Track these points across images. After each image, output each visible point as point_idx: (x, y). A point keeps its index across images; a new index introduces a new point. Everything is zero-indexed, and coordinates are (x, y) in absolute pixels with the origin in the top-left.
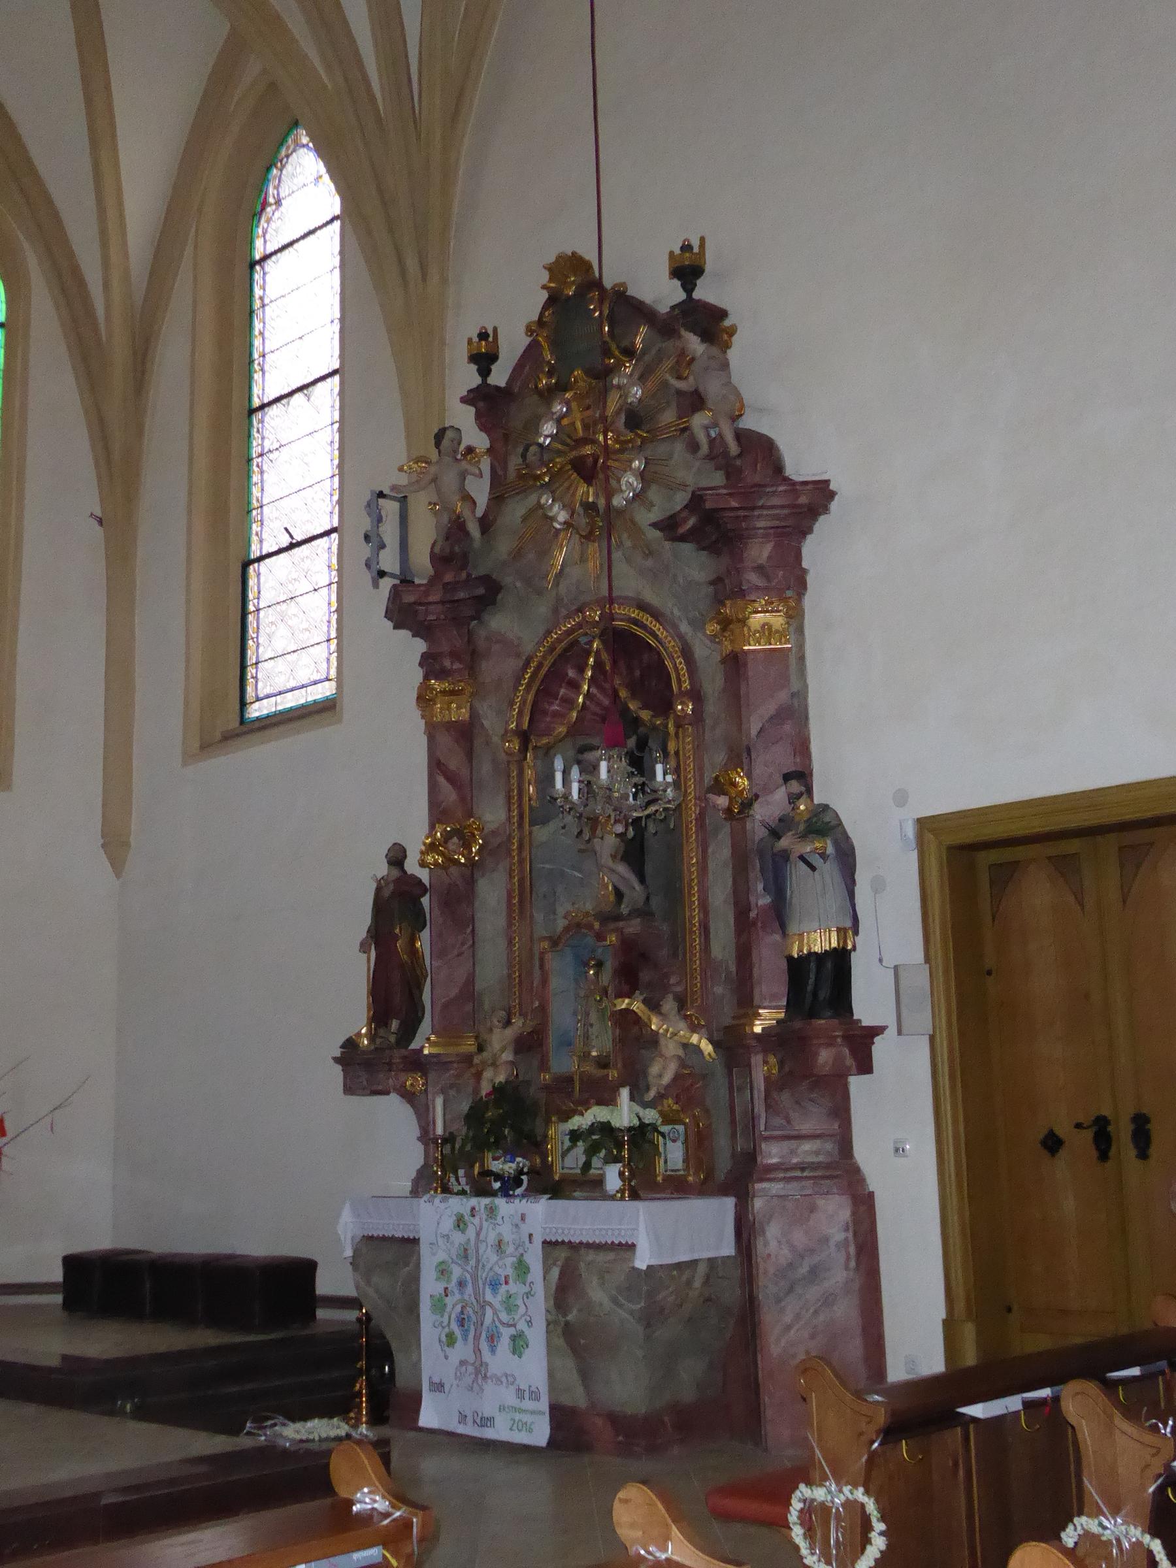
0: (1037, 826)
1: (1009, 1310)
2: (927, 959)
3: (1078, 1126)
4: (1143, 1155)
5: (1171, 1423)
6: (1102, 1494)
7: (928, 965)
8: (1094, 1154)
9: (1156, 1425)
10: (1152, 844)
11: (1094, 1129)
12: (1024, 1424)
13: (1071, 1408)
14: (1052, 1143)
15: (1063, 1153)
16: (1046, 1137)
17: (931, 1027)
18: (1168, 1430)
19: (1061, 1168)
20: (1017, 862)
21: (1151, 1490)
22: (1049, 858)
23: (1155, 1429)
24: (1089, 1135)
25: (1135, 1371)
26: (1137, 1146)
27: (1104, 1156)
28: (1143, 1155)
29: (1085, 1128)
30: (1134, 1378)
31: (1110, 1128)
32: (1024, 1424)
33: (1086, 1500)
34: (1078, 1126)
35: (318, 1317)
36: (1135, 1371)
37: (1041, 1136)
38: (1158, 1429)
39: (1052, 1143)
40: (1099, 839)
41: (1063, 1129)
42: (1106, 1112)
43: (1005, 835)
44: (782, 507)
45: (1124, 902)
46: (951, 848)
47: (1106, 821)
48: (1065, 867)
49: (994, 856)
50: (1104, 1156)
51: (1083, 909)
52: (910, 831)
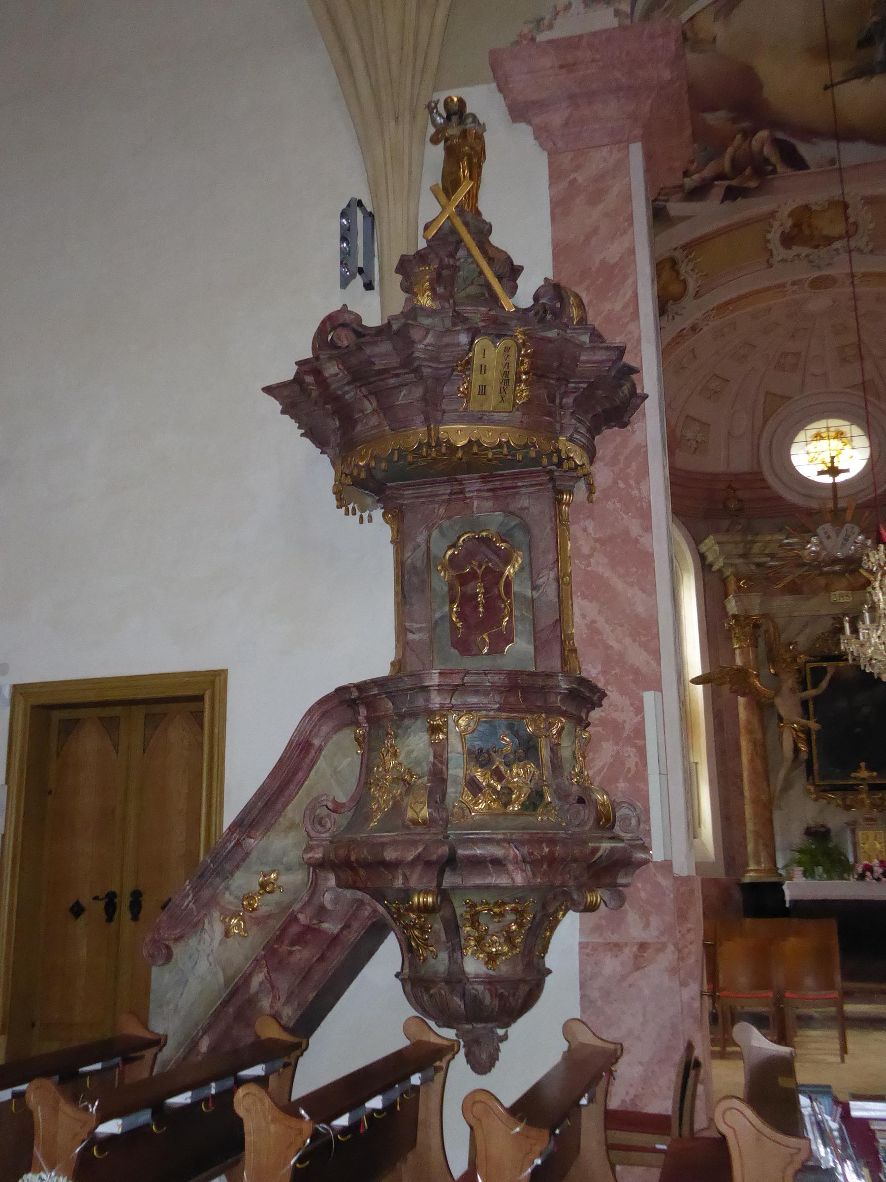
0: (92, 697)
1: (33, 1025)
2: (7, 782)
3: (96, 898)
4: (135, 917)
5: (97, 1103)
6: (44, 1156)
7: (7, 786)
8: (104, 916)
9: (87, 1106)
10: (165, 714)
11: (106, 900)
12: (13, 1109)
13: (32, 1099)
14: (77, 910)
15: (84, 917)
16: (73, 906)
17: (3, 830)
18: (94, 1108)
19: (81, 927)
20: (79, 719)
21: (78, 1150)
22: (100, 718)
23: (86, 1109)
24: (101, 905)
25: (98, 1066)
26: (132, 913)
27: (110, 918)
28: (135, 917)
29: (100, 900)
30: (97, 1071)
31: (116, 900)
32: (13, 1109)
33: (34, 1161)
34: (96, 898)
35: (746, 919)
36: (98, 1066)
37: (71, 905)
38: (88, 1109)
39: (77, 910)
40: (133, 708)
41: (86, 901)
42: (114, 888)
43: (118, 698)
44: (582, 442)
45: (144, 750)
46: (33, 707)
47: (139, 697)
48: (110, 726)
49: (66, 714)
50: (110, 918)
51: (117, 753)
52: (7, 693)
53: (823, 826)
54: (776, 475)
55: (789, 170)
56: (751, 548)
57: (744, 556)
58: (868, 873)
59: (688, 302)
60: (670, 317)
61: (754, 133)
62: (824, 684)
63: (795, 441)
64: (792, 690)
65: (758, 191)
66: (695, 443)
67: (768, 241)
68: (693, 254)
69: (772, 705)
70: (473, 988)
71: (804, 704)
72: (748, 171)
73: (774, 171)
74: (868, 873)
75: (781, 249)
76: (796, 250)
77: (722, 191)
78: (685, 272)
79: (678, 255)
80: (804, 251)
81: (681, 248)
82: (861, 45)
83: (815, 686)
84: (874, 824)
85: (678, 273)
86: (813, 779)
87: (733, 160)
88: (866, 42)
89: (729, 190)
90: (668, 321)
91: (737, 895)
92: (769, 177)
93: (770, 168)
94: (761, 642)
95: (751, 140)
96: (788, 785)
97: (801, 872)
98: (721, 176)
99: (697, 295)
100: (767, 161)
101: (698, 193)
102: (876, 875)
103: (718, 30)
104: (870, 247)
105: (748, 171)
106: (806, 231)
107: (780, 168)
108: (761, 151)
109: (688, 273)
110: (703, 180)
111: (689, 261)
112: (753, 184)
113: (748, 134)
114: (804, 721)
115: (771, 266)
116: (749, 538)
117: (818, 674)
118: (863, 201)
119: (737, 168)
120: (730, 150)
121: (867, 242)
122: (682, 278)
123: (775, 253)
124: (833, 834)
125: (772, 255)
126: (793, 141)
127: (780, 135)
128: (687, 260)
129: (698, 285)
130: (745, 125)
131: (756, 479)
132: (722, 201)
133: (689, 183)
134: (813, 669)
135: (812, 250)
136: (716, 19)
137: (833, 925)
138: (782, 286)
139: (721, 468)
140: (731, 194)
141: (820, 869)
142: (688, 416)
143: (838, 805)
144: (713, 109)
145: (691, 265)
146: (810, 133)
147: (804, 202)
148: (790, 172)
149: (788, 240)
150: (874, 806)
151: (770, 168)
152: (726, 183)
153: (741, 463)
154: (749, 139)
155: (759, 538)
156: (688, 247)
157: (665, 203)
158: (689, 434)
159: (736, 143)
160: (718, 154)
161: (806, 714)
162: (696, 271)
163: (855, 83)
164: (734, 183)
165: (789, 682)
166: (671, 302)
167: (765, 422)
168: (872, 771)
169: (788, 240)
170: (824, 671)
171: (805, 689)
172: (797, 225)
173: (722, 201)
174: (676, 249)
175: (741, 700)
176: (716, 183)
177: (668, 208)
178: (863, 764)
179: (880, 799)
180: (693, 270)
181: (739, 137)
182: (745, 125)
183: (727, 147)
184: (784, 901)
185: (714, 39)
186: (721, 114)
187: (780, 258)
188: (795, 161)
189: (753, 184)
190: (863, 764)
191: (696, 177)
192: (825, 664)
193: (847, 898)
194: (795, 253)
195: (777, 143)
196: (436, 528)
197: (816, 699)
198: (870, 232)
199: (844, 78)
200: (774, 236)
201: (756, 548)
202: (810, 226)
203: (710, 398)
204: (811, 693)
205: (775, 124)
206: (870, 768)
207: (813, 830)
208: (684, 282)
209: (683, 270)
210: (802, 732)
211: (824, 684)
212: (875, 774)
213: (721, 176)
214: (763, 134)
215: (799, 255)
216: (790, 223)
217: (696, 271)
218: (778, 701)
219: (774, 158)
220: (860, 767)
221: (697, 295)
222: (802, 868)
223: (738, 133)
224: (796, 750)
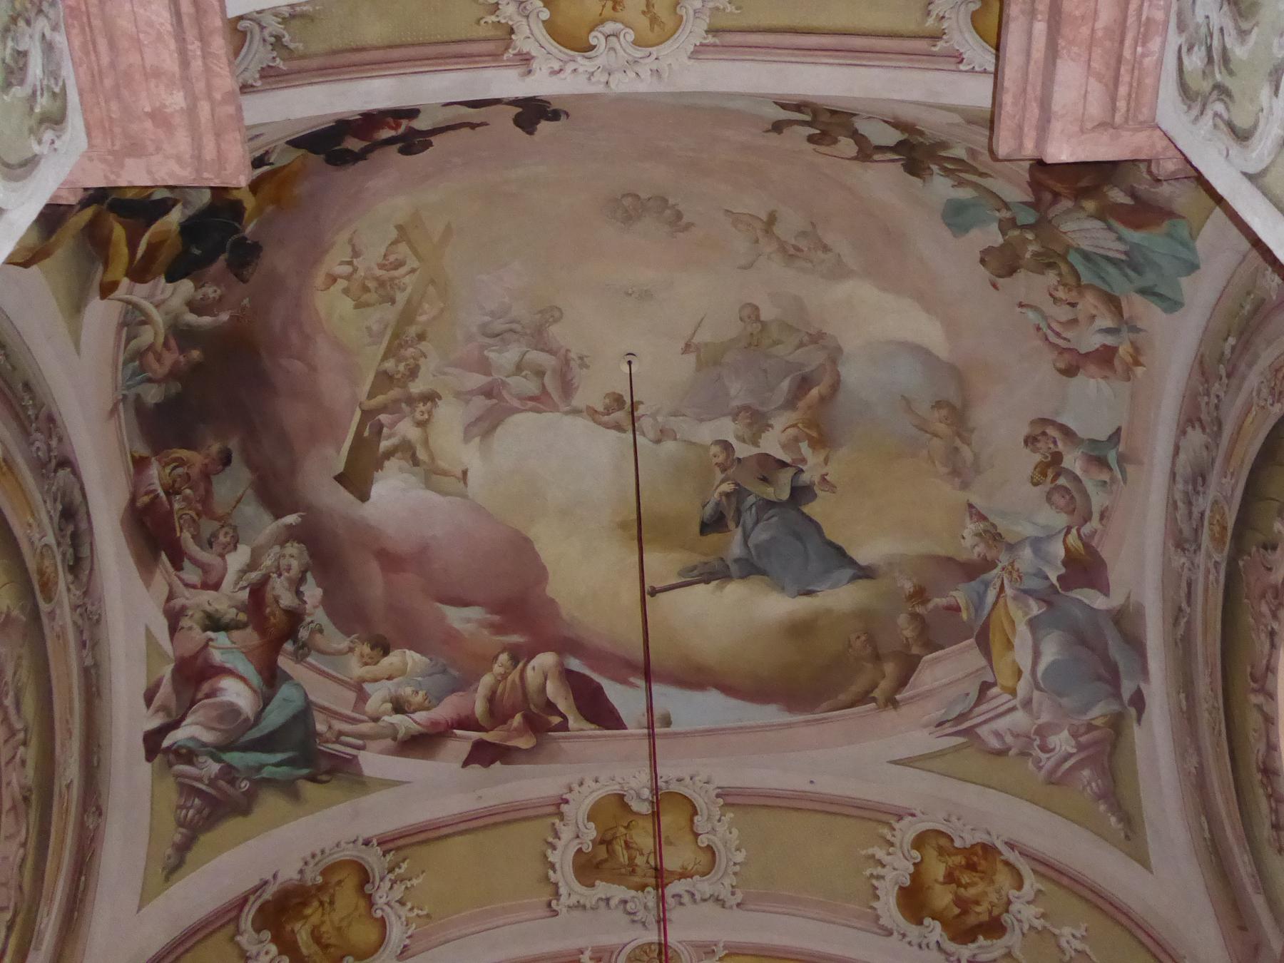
61: (531, 656)
65: (530, 755)
67: (552, 866)
68: (404, 866)
72: (518, 719)
73: (564, 726)
75: (577, 886)
76: (603, 888)
78: (388, 904)
79: (374, 860)
80: (618, 892)
81: (379, 844)
82: (705, 528)
84: (251, 32)
85: (371, 903)
87: (491, 699)
88: (714, 524)
98: (467, 723)
100: (551, 707)
103: (470, 456)
104: (739, 896)
106: (623, 856)
108: (543, 689)
109: (391, 907)
110: (435, 724)
112: (524, 742)
113: (519, 656)
118: (721, 801)
119: (497, 713)
120: (487, 680)
122: (379, 914)
123: (563, 890)
125: (557, 895)
126: (596, 677)
127: (575, 664)
128: (391, 876)
129: (409, 933)
130: (515, 639)
132: (466, 764)
136: (467, 438)
140: (483, 754)
145: (399, 891)
147: (615, 788)
148: (591, 730)
149: (588, 868)
151: (556, 720)
152: (475, 735)
154: (521, 665)
156: (392, 843)
157: (354, 752)
159: (497, 669)
160: (465, 684)
162: (409, 905)
163: (701, 591)
169: (588, 868)
172: (605, 841)
173: (466, 764)
174: (367, 843)
176: (458, 732)
177: (360, 758)
180: (402, 902)
181: (504, 657)
182: (515, 639)
185: (465, 473)
186: (475, 613)
189: (524, 742)
191: (421, 716)
195: (569, 677)
196: (181, 530)
198: (737, 868)
200: (563, 857)
202: (627, 846)
205: (567, 645)
208: (382, 922)
209: (380, 899)
213: (467, 723)
214: (546, 660)
215: (608, 900)
216: (591, 832)
217: (409, 905)
219: (564, 703)
223: (502, 652)
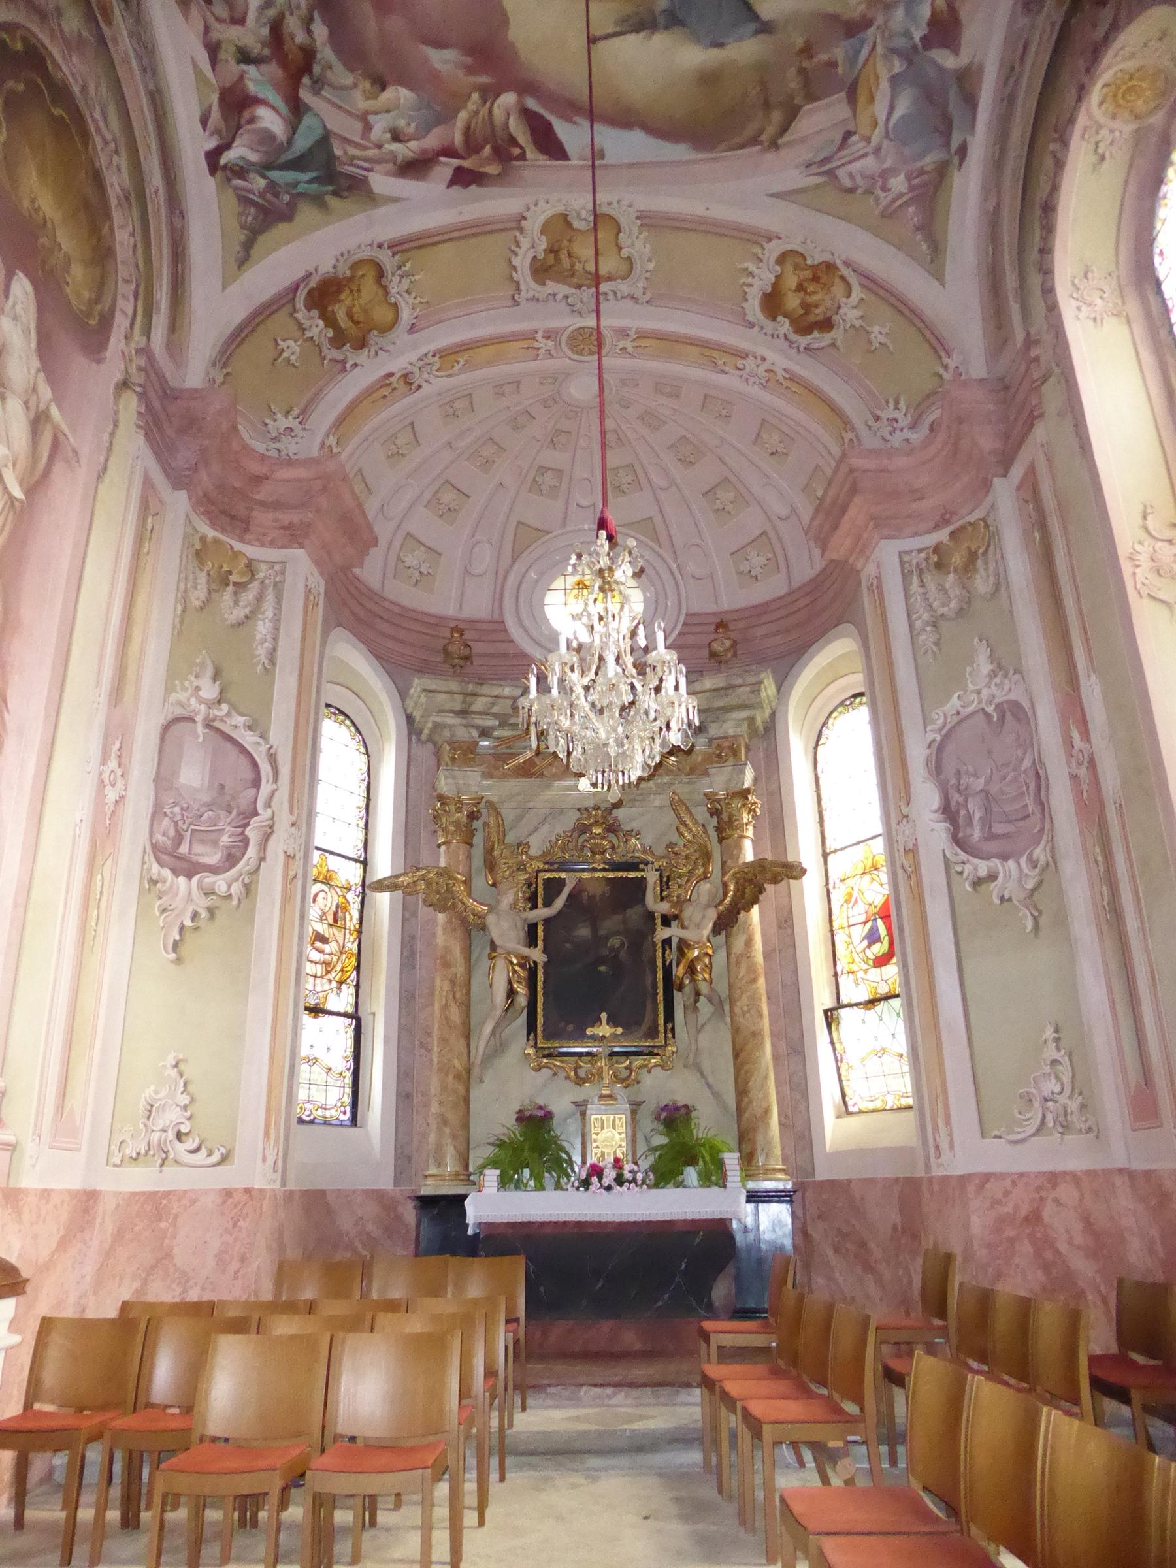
53: (540, 1108)
54: (520, 621)
55: (541, 157)
56: (471, 704)
57: (463, 713)
58: (595, 1179)
59: (400, 335)
60: (373, 352)
62: (560, 902)
63: (552, 587)
64: (514, 906)
66: (417, 574)
67: (515, 268)
68: (408, 265)
69: (483, 928)
70: (311, 1308)
71: (532, 929)
72: (487, 150)
73: (522, 157)
74: (595, 1179)
75: (533, 285)
76: (551, 287)
77: (448, 173)
79: (386, 259)
80: (562, 289)
83: (548, 903)
86: (536, 1039)
87: (467, 132)
89: (459, 170)
90: (369, 356)
91: (410, 1214)
92: (514, 163)
93: (517, 151)
94: (478, 840)
95: (492, 104)
96: (498, 1048)
97: (495, 1178)
98: (449, 152)
99: (412, 329)
100: (513, 141)
101: (414, 168)
102: (606, 1181)
105: (487, 150)
107: (531, 153)
108: (506, 125)
110: (424, 151)
111: (402, 277)
113: (489, 94)
114: (526, 951)
115: (516, 303)
116: (471, 687)
117: (553, 887)
119: (472, 146)
120: (463, 115)
121: (644, 289)
122: (393, 300)
123: (523, 287)
124: (555, 1121)
125: (518, 290)
126: (548, 115)
127: (531, 104)
128: (399, 272)
130: (484, 79)
131: (496, 628)
132: (448, 186)
133: (404, 151)
134: (547, 882)
135: (573, 290)
137: (517, 1269)
138: (530, 336)
139: (449, 609)
140: (462, 178)
141: (526, 1172)
142: (409, 535)
143: (567, 1078)
144: (439, 44)
145: (406, 283)
146: (571, 109)
148: (542, 160)
149: (542, 271)
150: (617, 1078)
151: (516, 151)
152: (456, 162)
153: (477, 606)
154: (488, 104)
155: (484, 690)
156: (399, 246)
157: (365, 173)
158: (410, 560)
159: (471, 106)
160: (444, 117)
161: (532, 941)
164: (466, 164)
165: (511, 895)
166: (375, 332)
167: (514, 560)
168: (616, 1025)
169: (542, 271)
170: (561, 883)
171: (534, 907)
172: (553, 251)
173: (448, 186)
174: (380, 246)
175: (441, 917)
176: (442, 159)
178: (604, 1016)
179: (626, 1068)
180: (408, 292)
181: (475, 96)
182: (484, 79)
183: (458, 111)
184: (467, 1226)
187: (530, 295)
188: (551, 147)
189: (493, 169)
190: (604, 1016)
191: (413, 145)
192: (563, 875)
193: (603, 1219)
194: (550, 291)
195: (529, 116)
197: (547, 921)
199: (618, 29)
200: (523, 262)
201: (479, 704)
203: (441, 516)
204: (542, 913)
205: (526, 87)
206: (612, 1021)
207: (527, 1113)
210: (522, 966)
211: (560, 902)
212: (619, 1030)
213: (449, 152)
214: (508, 99)
216: (543, 244)
217: (413, 295)
218: (491, 920)
219: (523, 137)
220: (600, 1020)
221: (412, 329)
222: (498, 1172)
224: (511, 993)
